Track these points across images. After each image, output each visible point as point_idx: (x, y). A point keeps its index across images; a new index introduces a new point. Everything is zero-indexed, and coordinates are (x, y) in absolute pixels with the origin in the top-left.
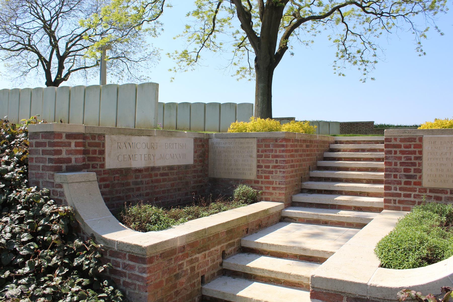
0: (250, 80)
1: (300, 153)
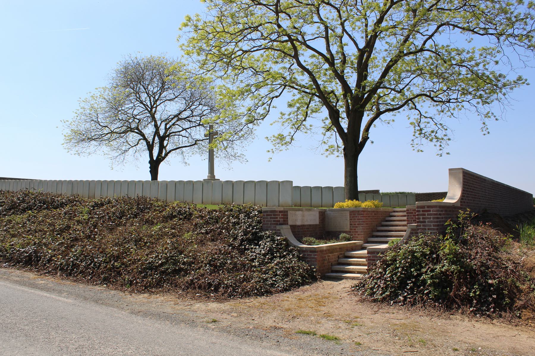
0: (338, 156)
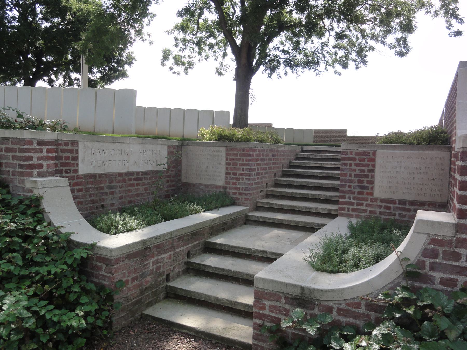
1: (265, 162)
